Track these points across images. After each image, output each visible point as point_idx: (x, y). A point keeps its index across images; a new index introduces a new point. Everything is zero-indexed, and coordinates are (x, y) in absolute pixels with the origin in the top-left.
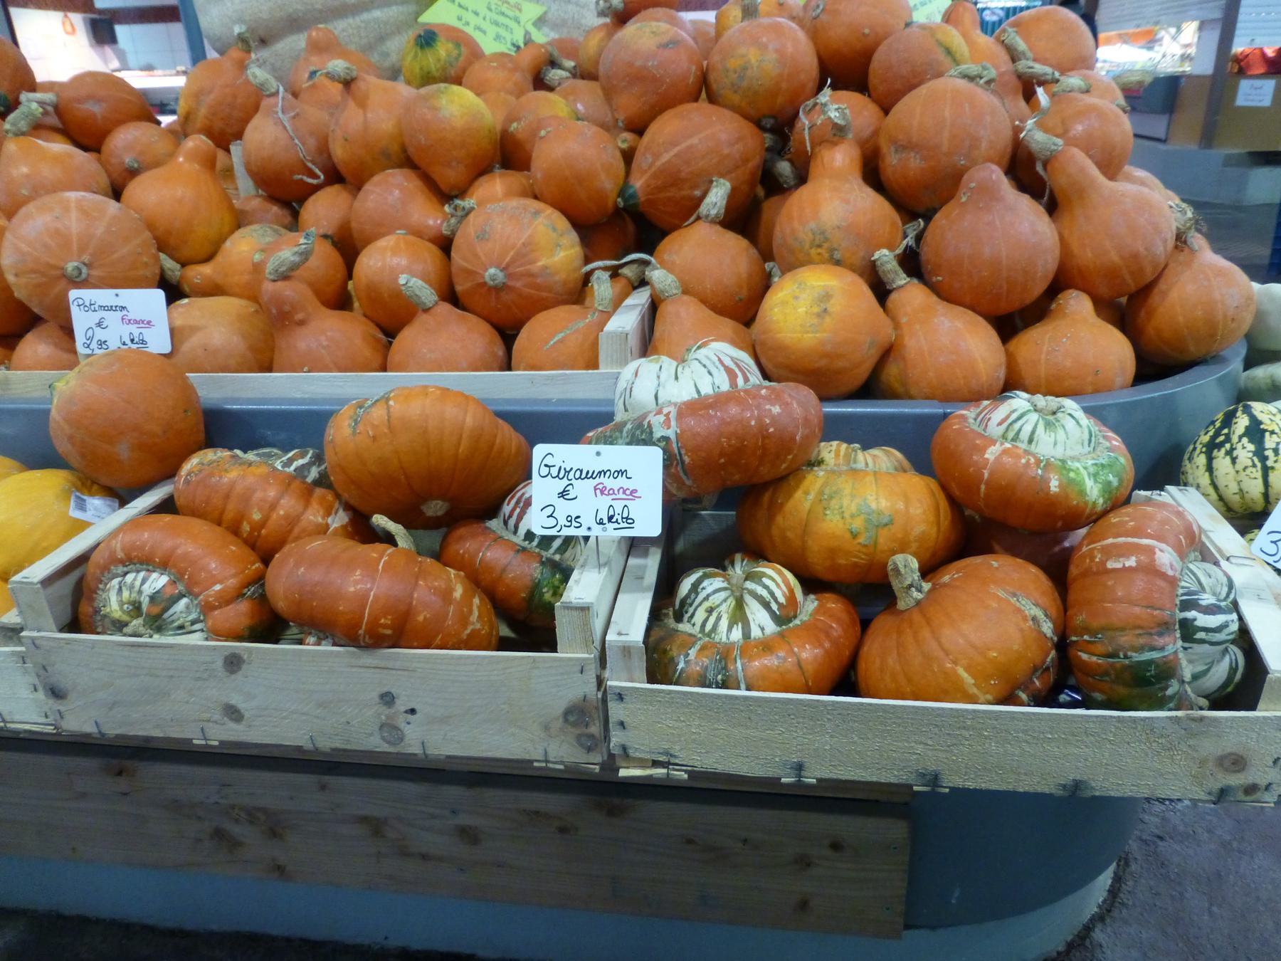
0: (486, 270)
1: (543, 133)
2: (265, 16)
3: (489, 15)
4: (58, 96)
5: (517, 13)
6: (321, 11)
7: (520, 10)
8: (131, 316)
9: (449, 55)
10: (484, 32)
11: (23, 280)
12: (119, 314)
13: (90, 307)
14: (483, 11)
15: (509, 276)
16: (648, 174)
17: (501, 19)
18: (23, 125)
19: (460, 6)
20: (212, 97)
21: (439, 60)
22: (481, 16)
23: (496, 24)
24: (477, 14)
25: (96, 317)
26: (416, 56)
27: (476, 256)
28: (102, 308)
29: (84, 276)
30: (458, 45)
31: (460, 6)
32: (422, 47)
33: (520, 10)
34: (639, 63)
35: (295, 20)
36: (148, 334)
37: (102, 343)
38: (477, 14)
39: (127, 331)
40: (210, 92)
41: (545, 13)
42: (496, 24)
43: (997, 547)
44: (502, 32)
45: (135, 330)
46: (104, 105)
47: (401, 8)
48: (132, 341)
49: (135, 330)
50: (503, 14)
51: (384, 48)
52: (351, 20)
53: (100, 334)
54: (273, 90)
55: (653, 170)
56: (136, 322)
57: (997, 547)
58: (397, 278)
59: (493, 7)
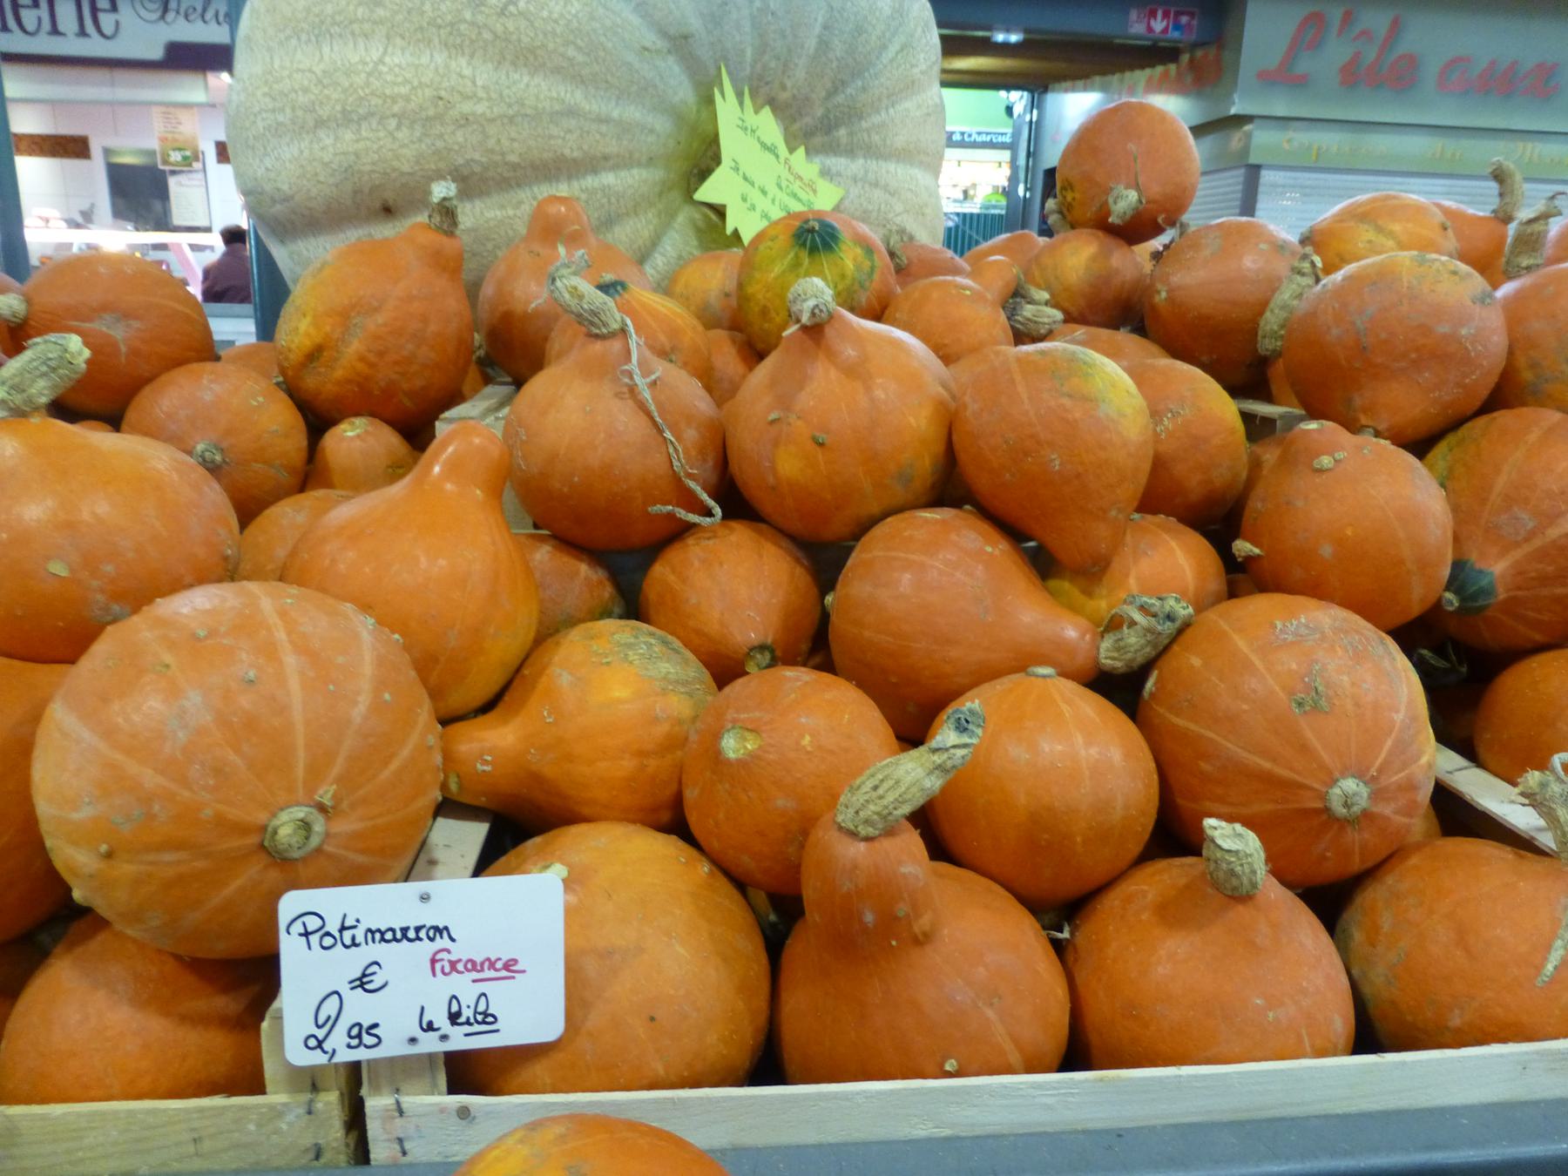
0: (1333, 782)
1: (1326, 461)
2: (406, 168)
4: (28, 301)
6: (515, 167)
7: (815, 191)
8: (459, 951)
9: (858, 267)
11: (126, 869)
12: (426, 948)
13: (343, 935)
14: (772, 190)
15: (1375, 796)
16: (1527, 548)
18: (42, 392)
19: (745, 178)
20: (380, 319)
21: (843, 276)
22: (770, 196)
24: (764, 192)
25: (351, 963)
27: (1304, 749)
28: (377, 935)
29: (315, 841)
31: (745, 178)
33: (815, 191)
34: (1443, 329)
36: (501, 997)
37: (362, 1033)
38: (764, 192)
39: (435, 995)
40: (376, 310)
45: (465, 988)
46: (136, 324)
48: (454, 1018)
49: (465, 988)
50: (795, 196)
53: (360, 1008)
54: (615, 326)
55: (1537, 542)
56: (473, 966)
59: (784, 184)
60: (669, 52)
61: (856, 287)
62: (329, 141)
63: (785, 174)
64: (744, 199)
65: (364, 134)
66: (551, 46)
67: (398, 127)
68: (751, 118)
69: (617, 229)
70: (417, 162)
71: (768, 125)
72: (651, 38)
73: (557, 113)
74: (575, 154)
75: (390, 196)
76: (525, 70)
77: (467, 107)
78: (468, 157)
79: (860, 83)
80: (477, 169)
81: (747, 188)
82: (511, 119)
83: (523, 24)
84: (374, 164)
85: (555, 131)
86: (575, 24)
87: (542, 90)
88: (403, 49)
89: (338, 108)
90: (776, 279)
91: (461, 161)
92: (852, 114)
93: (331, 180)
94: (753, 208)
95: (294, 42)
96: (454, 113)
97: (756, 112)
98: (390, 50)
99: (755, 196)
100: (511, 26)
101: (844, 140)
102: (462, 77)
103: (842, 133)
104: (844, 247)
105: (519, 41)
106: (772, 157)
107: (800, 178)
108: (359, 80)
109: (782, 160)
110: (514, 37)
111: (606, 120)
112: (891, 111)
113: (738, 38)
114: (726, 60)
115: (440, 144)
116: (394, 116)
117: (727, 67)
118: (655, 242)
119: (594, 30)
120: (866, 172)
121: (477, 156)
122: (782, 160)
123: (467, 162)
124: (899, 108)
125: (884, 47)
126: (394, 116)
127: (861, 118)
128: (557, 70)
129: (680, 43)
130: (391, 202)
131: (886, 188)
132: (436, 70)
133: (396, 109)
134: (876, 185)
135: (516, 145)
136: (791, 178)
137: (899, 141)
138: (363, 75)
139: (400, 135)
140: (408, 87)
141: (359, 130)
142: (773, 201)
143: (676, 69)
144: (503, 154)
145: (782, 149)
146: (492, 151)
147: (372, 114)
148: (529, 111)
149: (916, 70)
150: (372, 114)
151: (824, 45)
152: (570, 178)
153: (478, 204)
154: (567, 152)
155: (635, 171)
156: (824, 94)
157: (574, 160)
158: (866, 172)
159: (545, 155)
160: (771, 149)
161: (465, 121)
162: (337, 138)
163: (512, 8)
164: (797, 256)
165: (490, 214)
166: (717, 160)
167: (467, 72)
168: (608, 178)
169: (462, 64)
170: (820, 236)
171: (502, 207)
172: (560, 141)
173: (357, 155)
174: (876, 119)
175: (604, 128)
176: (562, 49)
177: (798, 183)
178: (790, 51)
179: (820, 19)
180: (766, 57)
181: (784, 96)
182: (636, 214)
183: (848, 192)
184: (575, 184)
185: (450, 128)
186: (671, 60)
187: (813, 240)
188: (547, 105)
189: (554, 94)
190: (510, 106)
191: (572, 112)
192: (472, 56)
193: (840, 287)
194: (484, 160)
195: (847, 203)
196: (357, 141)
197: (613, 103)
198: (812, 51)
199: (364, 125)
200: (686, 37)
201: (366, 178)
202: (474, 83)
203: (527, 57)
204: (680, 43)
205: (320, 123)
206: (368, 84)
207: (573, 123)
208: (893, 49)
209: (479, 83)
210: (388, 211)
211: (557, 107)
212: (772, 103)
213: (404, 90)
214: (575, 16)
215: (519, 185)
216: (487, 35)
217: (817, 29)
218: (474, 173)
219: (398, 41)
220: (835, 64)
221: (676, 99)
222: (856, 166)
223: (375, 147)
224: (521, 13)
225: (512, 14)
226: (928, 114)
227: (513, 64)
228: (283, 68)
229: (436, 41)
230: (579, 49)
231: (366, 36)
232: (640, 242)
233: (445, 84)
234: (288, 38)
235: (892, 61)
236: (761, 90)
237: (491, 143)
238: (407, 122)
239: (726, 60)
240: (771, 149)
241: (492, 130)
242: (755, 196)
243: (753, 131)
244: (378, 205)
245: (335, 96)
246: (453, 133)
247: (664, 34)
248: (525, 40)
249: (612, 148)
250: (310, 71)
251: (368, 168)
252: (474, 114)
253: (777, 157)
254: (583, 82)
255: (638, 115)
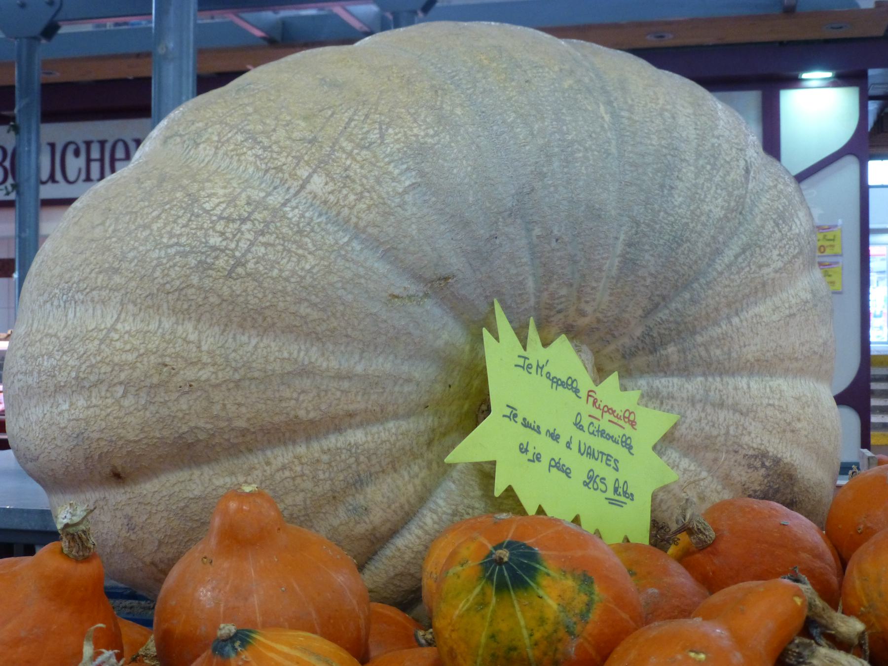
2: (131, 436)
3: (580, 437)
5: (628, 430)
6: (244, 432)
7: (633, 424)
9: (565, 607)
10: (567, 472)
14: (567, 431)
17: (599, 444)
19: (526, 424)
21: (542, 621)
22: (563, 441)
23: (590, 453)
26: (482, 604)
30: (586, 580)
31: (526, 424)
32: (501, 588)
33: (633, 424)
35: (190, 446)
38: (555, 437)
41: (675, 426)
42: (590, 453)
43: (249, 67)
44: (601, 469)
47: (404, 425)
50: (602, 433)
51: (360, 499)
52: (301, 449)
57: (249, 67)
58: (216, 627)
59: (585, 422)
60: (426, 295)
61: (561, 633)
62: (65, 407)
63: (587, 409)
64: (523, 450)
65: (94, 401)
66: (281, 305)
67: (124, 396)
68: (536, 351)
69: (369, 490)
70: (142, 430)
71: (564, 357)
72: (403, 285)
73: (289, 373)
74: (312, 415)
75: (118, 463)
76: (253, 332)
77: (190, 374)
78: (192, 424)
79: (687, 296)
80: (202, 436)
81: (527, 436)
82: (237, 384)
83: (251, 285)
84: (102, 431)
85: (287, 393)
86: (309, 280)
87: (272, 351)
88: (134, 316)
89: (73, 374)
90: (461, 616)
91: (185, 428)
92: (682, 330)
93: (67, 445)
94: (538, 458)
95: (48, 305)
96: (178, 379)
97: (545, 344)
98: (123, 316)
99: (540, 443)
100: (238, 288)
101: (675, 358)
102: (189, 342)
103: (671, 349)
104: (544, 581)
105: (247, 302)
106: (570, 394)
107: (611, 411)
108: (92, 346)
109: (583, 394)
110: (241, 299)
111: (349, 377)
112: (735, 320)
113: (513, 271)
114: (499, 294)
115: (164, 411)
116: (121, 383)
117: (501, 302)
118: (423, 499)
119: (331, 284)
120: (707, 391)
121: (201, 424)
122: (583, 394)
123: (192, 430)
124: (749, 314)
125: (718, 252)
126: (121, 383)
127: (694, 333)
128: (289, 329)
129: (439, 285)
130: (120, 470)
131: (735, 408)
132: (163, 335)
133: (123, 376)
134: (722, 405)
135: (243, 410)
136: (597, 413)
137: (750, 353)
138: (97, 342)
139: (126, 403)
140: (135, 354)
141: (90, 397)
142: (568, 445)
143: (437, 311)
144: (229, 420)
145: (585, 381)
146: (217, 417)
147: (102, 382)
148: (256, 374)
149: (765, 270)
150: (102, 382)
151: (629, 263)
152: (308, 439)
153: (207, 471)
154: (302, 413)
155: (391, 425)
156: (640, 312)
157: (312, 422)
158: (707, 391)
159: (276, 419)
160: (570, 385)
161: (190, 387)
162: (71, 404)
163: (240, 270)
164: (483, 593)
165: (218, 482)
166: (489, 411)
167: (193, 337)
168: (357, 436)
169: (188, 329)
170: (510, 569)
171: (233, 473)
172: (293, 402)
173: (87, 421)
174: (716, 331)
175: (346, 385)
176: (293, 308)
177: (607, 416)
178: (583, 276)
179: (622, 237)
180: (553, 286)
181: (583, 322)
182: (395, 470)
183: (684, 416)
184: (315, 446)
185: (174, 396)
186: (429, 304)
187: (501, 570)
188: (277, 366)
189: (286, 355)
190: (236, 370)
191: (305, 372)
192: (199, 320)
193: (537, 635)
194: (209, 426)
195: (683, 429)
196: (88, 407)
197: (357, 357)
198: (614, 272)
199: (95, 391)
200: (446, 279)
201: (94, 445)
202: (199, 347)
203: (257, 319)
204: (439, 285)
205: (59, 389)
206: (99, 351)
207: (307, 383)
208: (729, 255)
209: (205, 348)
210: (118, 477)
211: (289, 368)
212: (572, 332)
213: (131, 357)
214: (309, 271)
215: (250, 451)
216: (213, 299)
217: (620, 248)
218: (199, 441)
219: (130, 307)
220: (649, 281)
221: (440, 343)
222: (694, 385)
223: (104, 413)
224: (249, 275)
225: (239, 276)
226: (792, 315)
227: (241, 326)
228: (38, 331)
229: (165, 306)
230: (314, 305)
231: (103, 302)
232: (403, 500)
233: (170, 351)
234: (45, 302)
235: (729, 266)
236: (548, 319)
237: (216, 409)
238: (132, 390)
239: (499, 294)
240: (570, 385)
241: (217, 396)
242: (540, 443)
243: (540, 367)
244: (108, 470)
245: (71, 363)
246: (177, 400)
247: (418, 278)
248: (253, 301)
249: (359, 404)
250: (55, 335)
251: (96, 435)
252: (197, 380)
253: (576, 391)
254: (318, 339)
255: (388, 366)
